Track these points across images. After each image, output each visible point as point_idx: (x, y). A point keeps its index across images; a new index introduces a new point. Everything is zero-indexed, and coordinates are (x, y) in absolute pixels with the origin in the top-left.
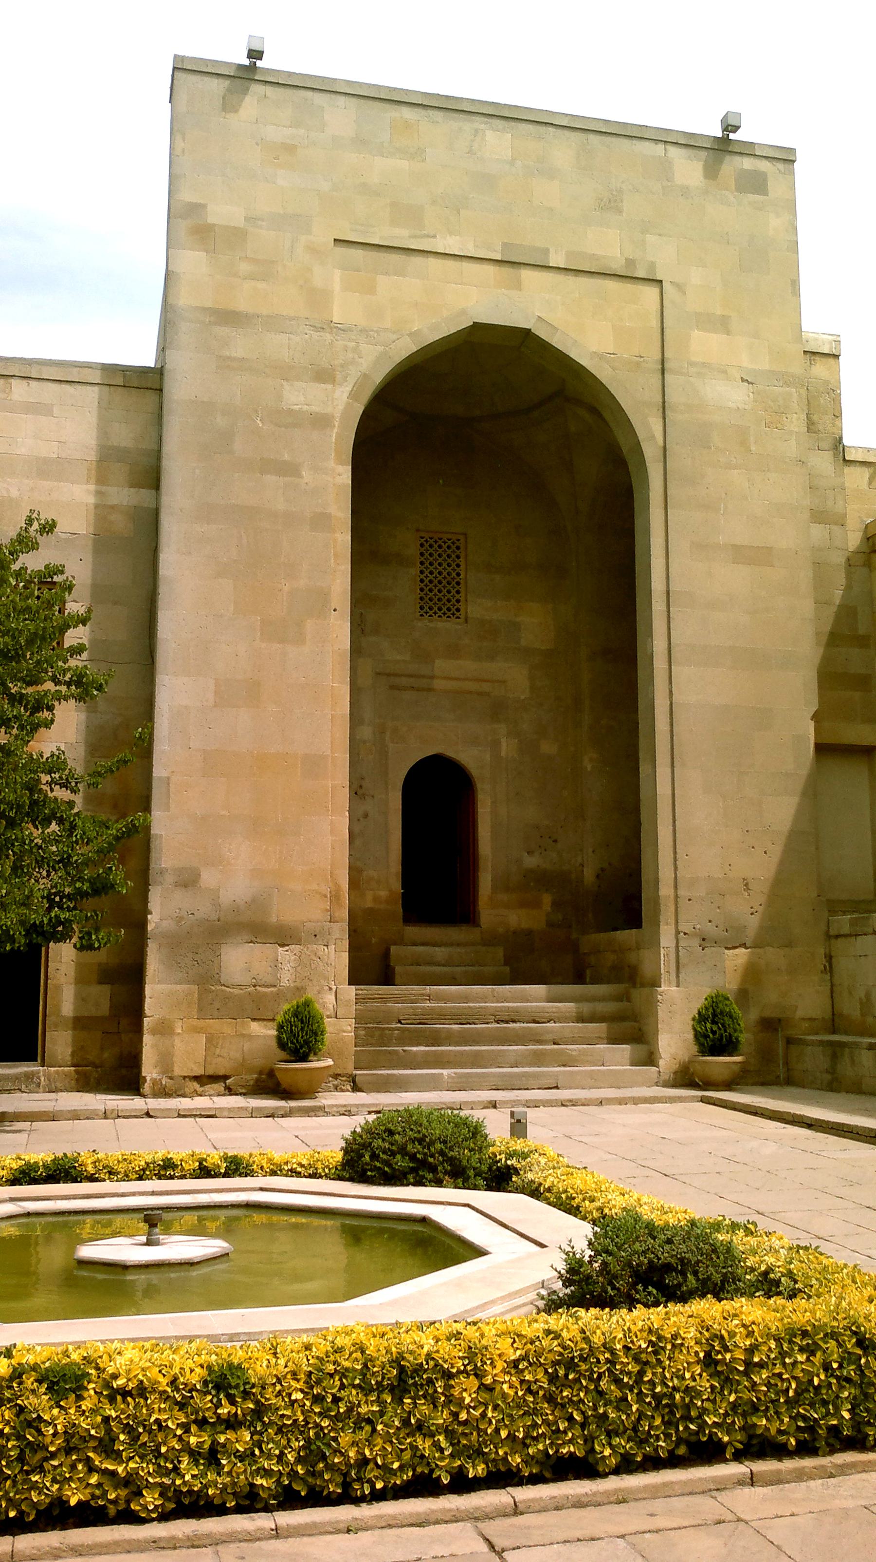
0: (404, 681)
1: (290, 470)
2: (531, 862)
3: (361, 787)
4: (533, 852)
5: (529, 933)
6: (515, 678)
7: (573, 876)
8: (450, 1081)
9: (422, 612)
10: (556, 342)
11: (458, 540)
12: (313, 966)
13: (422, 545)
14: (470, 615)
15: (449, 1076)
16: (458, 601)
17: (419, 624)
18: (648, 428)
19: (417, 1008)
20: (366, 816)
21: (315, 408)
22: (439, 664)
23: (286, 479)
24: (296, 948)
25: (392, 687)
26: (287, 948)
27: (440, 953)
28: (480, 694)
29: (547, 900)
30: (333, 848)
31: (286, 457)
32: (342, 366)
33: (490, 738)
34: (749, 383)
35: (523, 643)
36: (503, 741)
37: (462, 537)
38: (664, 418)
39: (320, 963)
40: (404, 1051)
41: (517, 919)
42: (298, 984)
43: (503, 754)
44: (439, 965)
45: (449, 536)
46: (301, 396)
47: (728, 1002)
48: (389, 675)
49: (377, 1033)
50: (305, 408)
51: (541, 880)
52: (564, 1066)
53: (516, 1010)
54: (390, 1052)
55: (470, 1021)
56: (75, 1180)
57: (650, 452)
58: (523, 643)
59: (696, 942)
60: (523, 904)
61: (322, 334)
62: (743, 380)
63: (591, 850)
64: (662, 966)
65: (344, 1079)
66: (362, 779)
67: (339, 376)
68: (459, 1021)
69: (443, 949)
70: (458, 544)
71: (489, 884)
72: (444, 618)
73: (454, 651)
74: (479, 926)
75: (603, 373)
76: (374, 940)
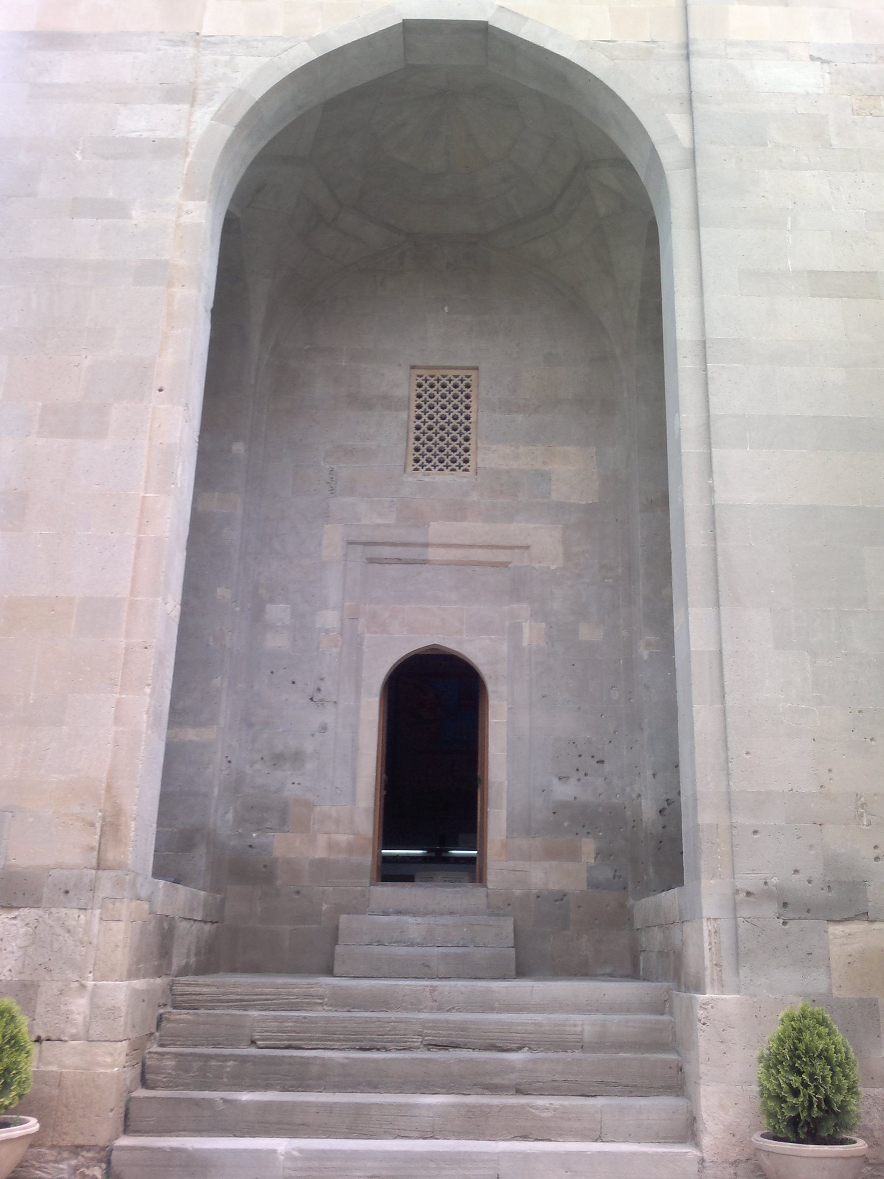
0: (387, 552)
1: (116, 209)
2: (564, 791)
3: (319, 690)
4: (567, 778)
5: (562, 897)
6: (543, 542)
7: (629, 813)
8: (288, 1164)
9: (417, 465)
10: (525, 33)
11: (468, 377)
12: (56, 946)
13: (420, 386)
14: (480, 465)
15: (288, 1156)
16: (466, 450)
17: (410, 479)
18: (666, 130)
19: (288, 1019)
20: (324, 728)
21: (158, 134)
22: (438, 530)
23: (105, 221)
24: (29, 914)
25: (372, 561)
26: (15, 913)
27: (414, 926)
29: (589, 847)
30: (117, 744)
31: (110, 194)
32: (207, 83)
33: (507, 624)
34: (824, 62)
35: (555, 496)
38: (692, 113)
39: (70, 942)
40: (225, 1101)
41: (543, 876)
42: (26, 977)
43: (525, 643)
44: (412, 945)
45: (456, 372)
46: (143, 121)
47: (823, 1030)
48: (365, 544)
49: (196, 1065)
50: (145, 135)
51: (582, 818)
52: (525, 1137)
53: (462, 1027)
54: (196, 1103)
55: (379, 1045)
57: (669, 156)
58: (555, 496)
59: (770, 910)
60: (551, 854)
61: (181, 48)
62: (812, 58)
63: (649, 773)
64: (707, 951)
65: (90, 1155)
66: (322, 679)
67: (201, 96)
68: (358, 1045)
69: (419, 920)
70: (467, 381)
71: (504, 825)
72: (447, 471)
73: (457, 510)
74: (486, 886)
75: (597, 66)
76: (325, 907)
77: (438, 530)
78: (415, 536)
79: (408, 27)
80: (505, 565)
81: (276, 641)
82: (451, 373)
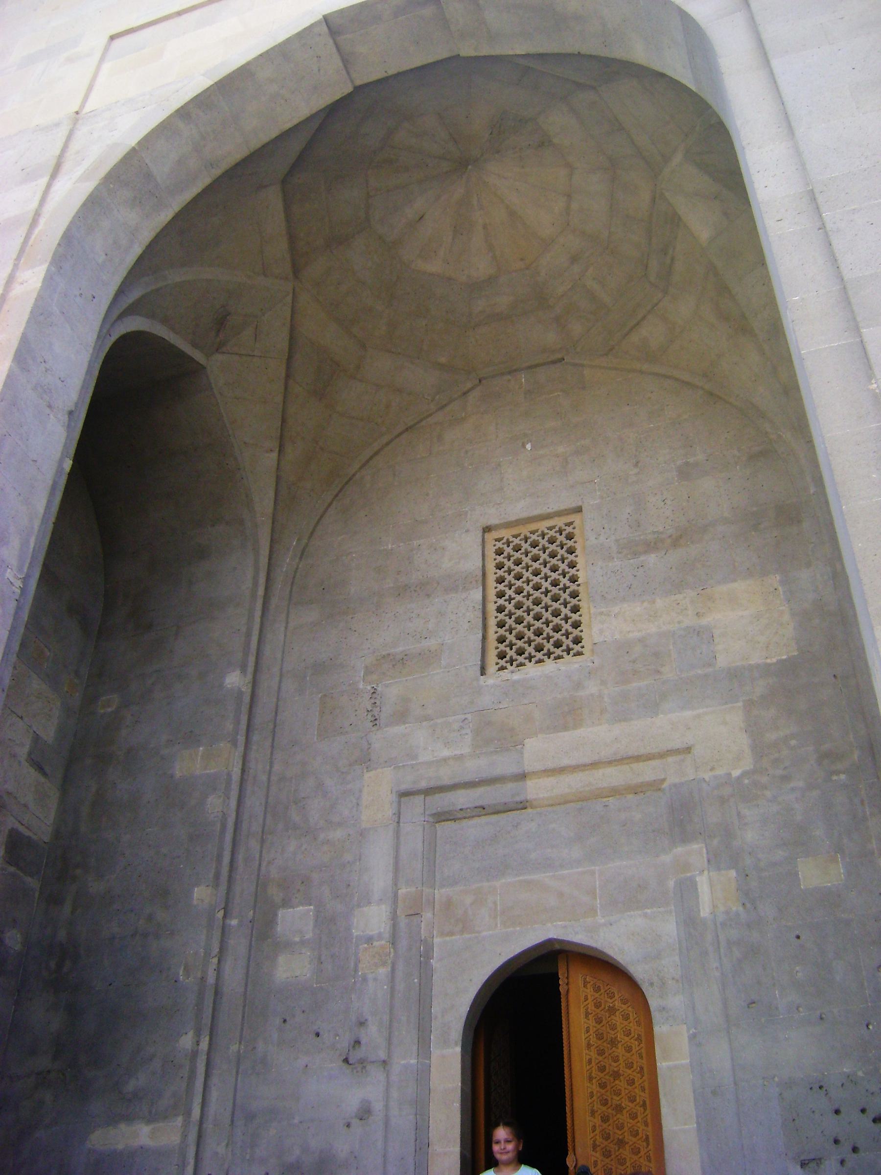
0: (462, 799)
3: (357, 1042)
28: (636, 790)
35: (722, 661)
37: (491, 537)
43: (705, 911)
48: (429, 792)
56: (31, 563)
70: (569, 529)
73: (567, 714)
77: (538, 750)
78: (505, 765)
79: (550, 941)
80: (656, 786)
81: (291, 968)
82: (543, 526)
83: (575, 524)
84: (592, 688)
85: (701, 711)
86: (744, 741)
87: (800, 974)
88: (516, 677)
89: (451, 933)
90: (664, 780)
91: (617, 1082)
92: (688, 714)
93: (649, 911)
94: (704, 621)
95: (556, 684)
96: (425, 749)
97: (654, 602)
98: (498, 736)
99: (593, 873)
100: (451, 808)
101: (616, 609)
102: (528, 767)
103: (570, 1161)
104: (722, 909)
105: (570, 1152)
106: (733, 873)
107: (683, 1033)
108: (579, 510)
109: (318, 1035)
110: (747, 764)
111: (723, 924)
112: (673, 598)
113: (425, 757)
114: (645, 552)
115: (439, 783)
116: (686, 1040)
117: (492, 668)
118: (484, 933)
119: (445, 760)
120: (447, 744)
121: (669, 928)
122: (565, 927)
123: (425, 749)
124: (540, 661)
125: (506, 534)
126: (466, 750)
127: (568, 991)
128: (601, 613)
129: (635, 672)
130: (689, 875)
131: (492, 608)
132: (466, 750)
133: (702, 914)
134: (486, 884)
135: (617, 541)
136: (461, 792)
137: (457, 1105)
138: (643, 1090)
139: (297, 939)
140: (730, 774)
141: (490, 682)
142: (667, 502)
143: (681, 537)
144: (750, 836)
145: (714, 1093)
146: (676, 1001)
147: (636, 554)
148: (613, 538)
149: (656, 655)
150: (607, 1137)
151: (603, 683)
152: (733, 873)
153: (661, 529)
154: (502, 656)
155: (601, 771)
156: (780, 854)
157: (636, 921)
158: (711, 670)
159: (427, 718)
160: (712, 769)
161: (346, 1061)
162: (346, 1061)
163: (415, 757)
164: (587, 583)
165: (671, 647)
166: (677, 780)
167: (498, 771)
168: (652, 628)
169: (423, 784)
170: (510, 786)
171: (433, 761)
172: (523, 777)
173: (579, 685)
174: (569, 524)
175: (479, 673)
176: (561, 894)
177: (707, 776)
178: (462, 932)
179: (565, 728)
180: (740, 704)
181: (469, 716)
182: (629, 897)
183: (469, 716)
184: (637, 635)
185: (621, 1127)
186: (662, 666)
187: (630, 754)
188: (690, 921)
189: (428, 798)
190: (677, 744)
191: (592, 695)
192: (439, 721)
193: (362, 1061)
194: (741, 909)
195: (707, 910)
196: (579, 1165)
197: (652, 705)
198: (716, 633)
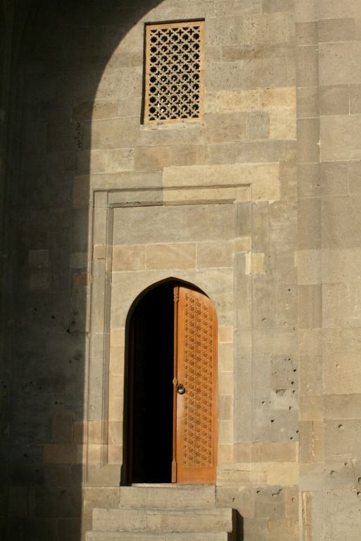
0: (128, 197)
3: (74, 322)
35: (272, 136)
36: (248, 257)
37: (149, 28)
43: (248, 272)
58: (272, 136)
70: (196, 32)
73: (187, 156)
78: (152, 181)
79: (171, 277)
80: (230, 201)
82: (180, 26)
83: (200, 29)
84: (202, 141)
85: (257, 164)
86: (278, 184)
87: (288, 308)
88: (160, 128)
89: (121, 270)
90: (234, 200)
91: (195, 6)
92: (251, 164)
93: (221, 268)
94: (265, 110)
95: (182, 137)
96: (109, 166)
97: (240, 93)
98: (149, 163)
99: (195, 245)
100: (122, 201)
101: (218, 94)
102: (164, 185)
103: (174, 382)
104: (256, 272)
105: (175, 378)
106: (263, 255)
107: (232, 329)
108: (203, 20)
109: (53, 317)
110: (277, 197)
111: (256, 280)
112: (251, 91)
113: (108, 171)
114: (238, 58)
115: (117, 188)
116: (233, 332)
117: (147, 119)
118: (137, 271)
119: (119, 174)
120: (121, 164)
121: (230, 278)
122: (179, 272)
123: (109, 166)
124: (174, 118)
125: (159, 28)
126: (131, 169)
127: (178, 301)
128: (210, 95)
129: (226, 135)
130: (242, 252)
131: (148, 78)
132: (131, 169)
133: (246, 273)
134: (139, 245)
135: (223, 47)
136: (128, 193)
137: (123, 355)
138: (211, 335)
139: (40, 267)
140: (268, 202)
141: (146, 129)
142: (255, 25)
143: (259, 51)
144: (274, 236)
145: (242, 358)
146: (230, 314)
147: (233, 59)
148: (221, 45)
149: (238, 126)
150: (192, 309)
151: (208, 139)
152: (263, 255)
153: (249, 43)
154: (152, 110)
155: (203, 190)
156: (287, 248)
157: (214, 272)
158: (265, 140)
159: (110, 147)
160: (260, 198)
161: (68, 331)
162: (68, 331)
163: (103, 170)
164: (203, 70)
165: (246, 123)
166: (241, 201)
167: (148, 185)
168: (237, 109)
169: (107, 187)
170: (154, 192)
171: (112, 174)
172: (162, 189)
173: (194, 139)
174: (196, 28)
175: (139, 122)
176: (177, 255)
177: (256, 201)
178: (127, 269)
179: (186, 164)
180: (278, 163)
181: (133, 149)
182: (213, 260)
183: (133, 149)
184: (229, 112)
185: (199, 336)
186: (240, 133)
187: (219, 184)
188: (240, 276)
189: (110, 194)
190: (243, 181)
191: (202, 146)
192: (117, 149)
193: (76, 332)
194: (265, 273)
195: (249, 272)
196: (179, 383)
197: (233, 158)
198: (272, 117)
